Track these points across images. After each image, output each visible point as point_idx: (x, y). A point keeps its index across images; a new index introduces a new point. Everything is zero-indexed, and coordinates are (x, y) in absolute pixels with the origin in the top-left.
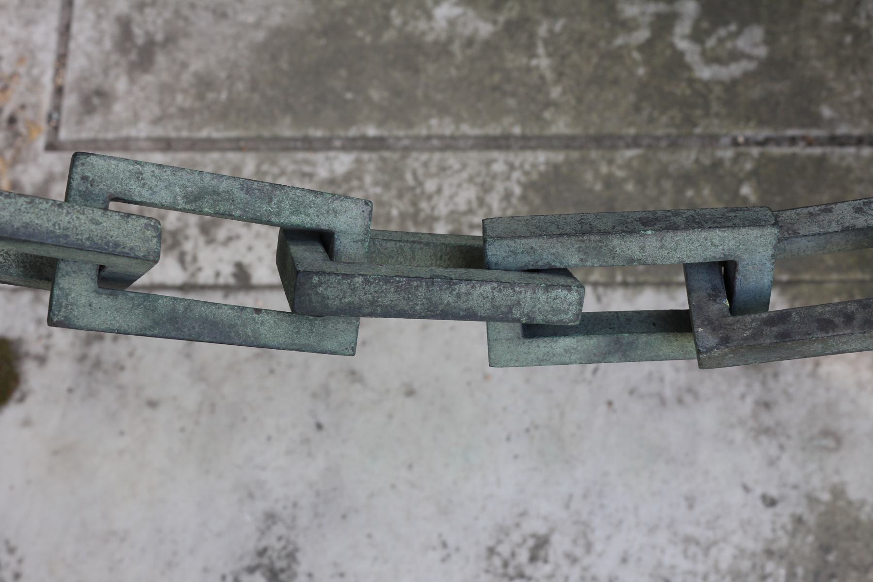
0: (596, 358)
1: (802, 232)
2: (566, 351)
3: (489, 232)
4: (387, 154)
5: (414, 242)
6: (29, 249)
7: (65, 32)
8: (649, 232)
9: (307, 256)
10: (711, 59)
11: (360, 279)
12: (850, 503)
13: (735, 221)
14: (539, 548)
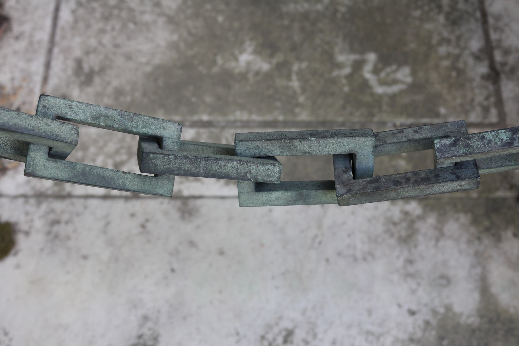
0: (291, 203)
1: (389, 142)
2: (276, 199)
3: (237, 139)
4: (213, 130)
5: (203, 146)
6: (17, 136)
7: (48, 66)
8: (313, 139)
9: (148, 147)
10: (383, 83)
11: (173, 157)
12: (455, 314)
13: (354, 134)
14: (289, 335)
